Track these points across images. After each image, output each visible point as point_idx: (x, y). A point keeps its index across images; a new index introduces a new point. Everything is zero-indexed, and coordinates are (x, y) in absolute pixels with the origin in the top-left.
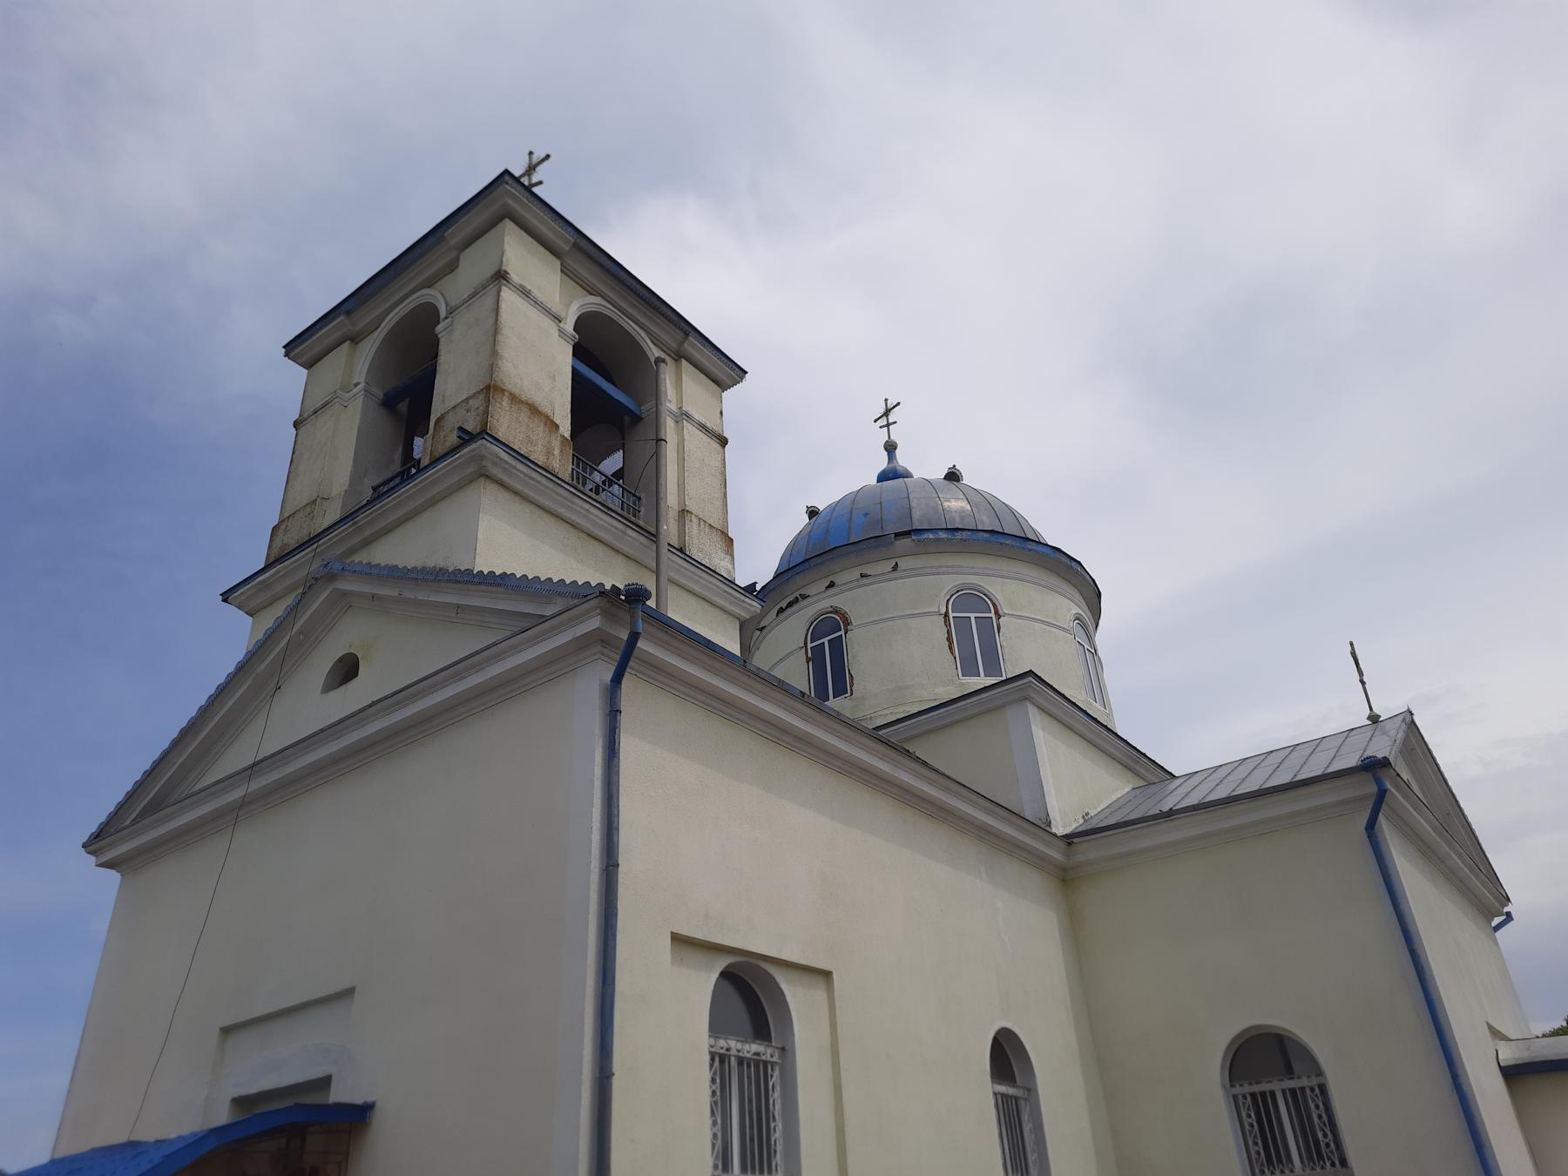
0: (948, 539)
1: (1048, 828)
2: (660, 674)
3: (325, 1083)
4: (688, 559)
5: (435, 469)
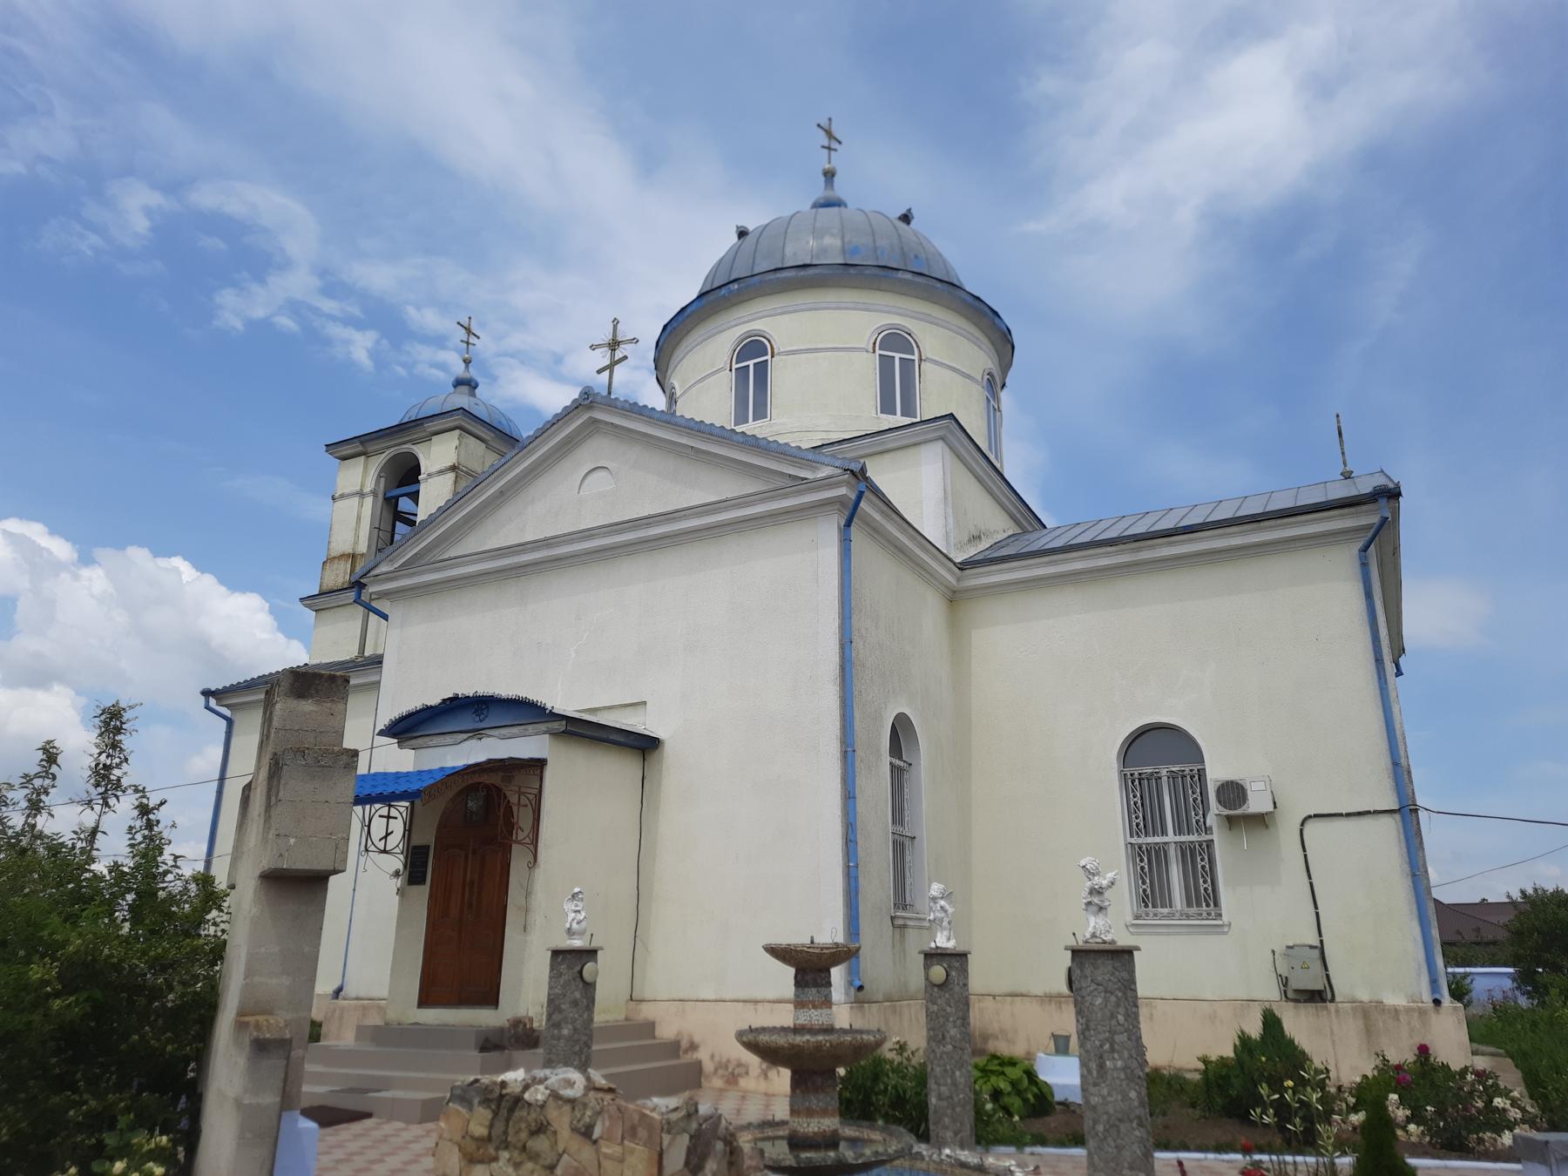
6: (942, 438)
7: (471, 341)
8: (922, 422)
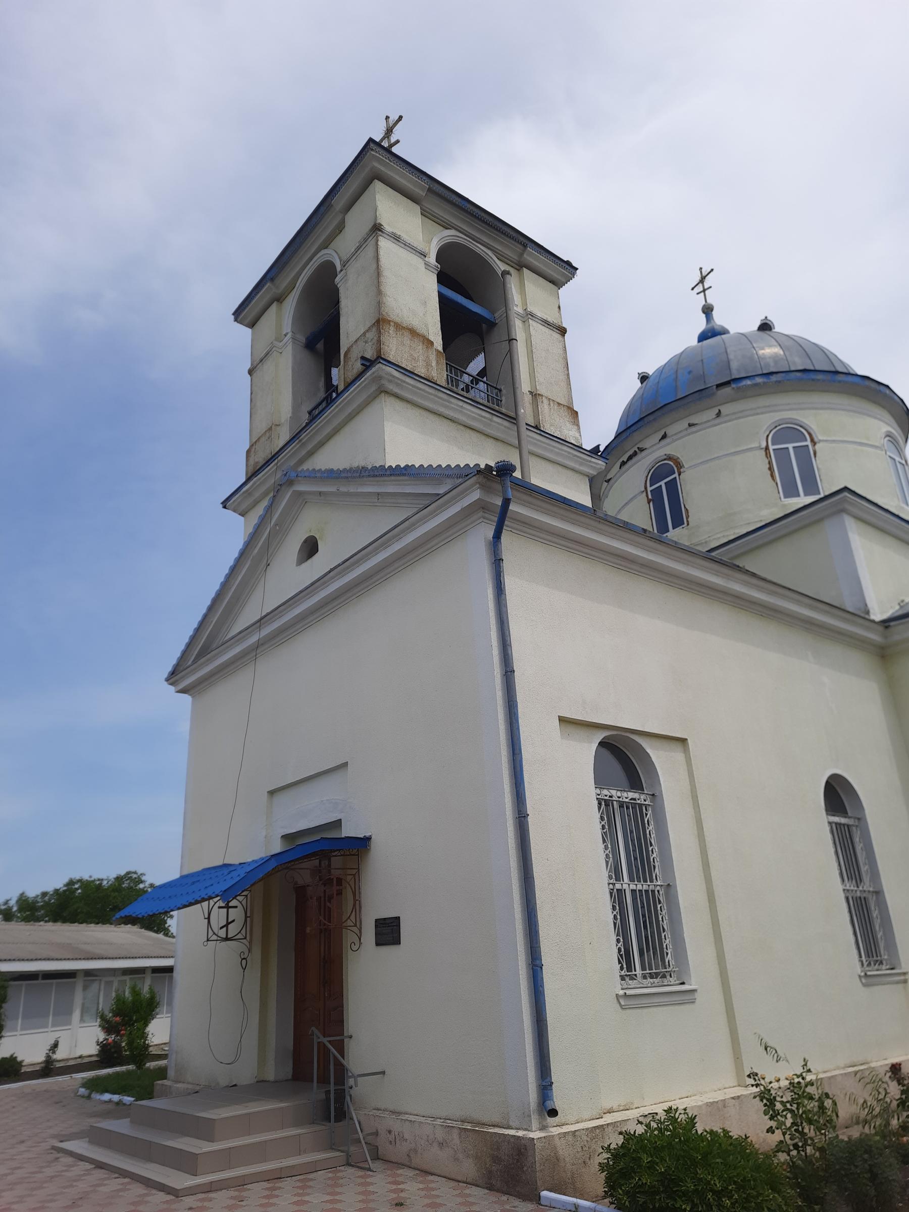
0: (764, 383)
1: (867, 616)
2: (530, 528)
3: (337, 824)
4: (543, 434)
5: (349, 392)
8: (826, 497)
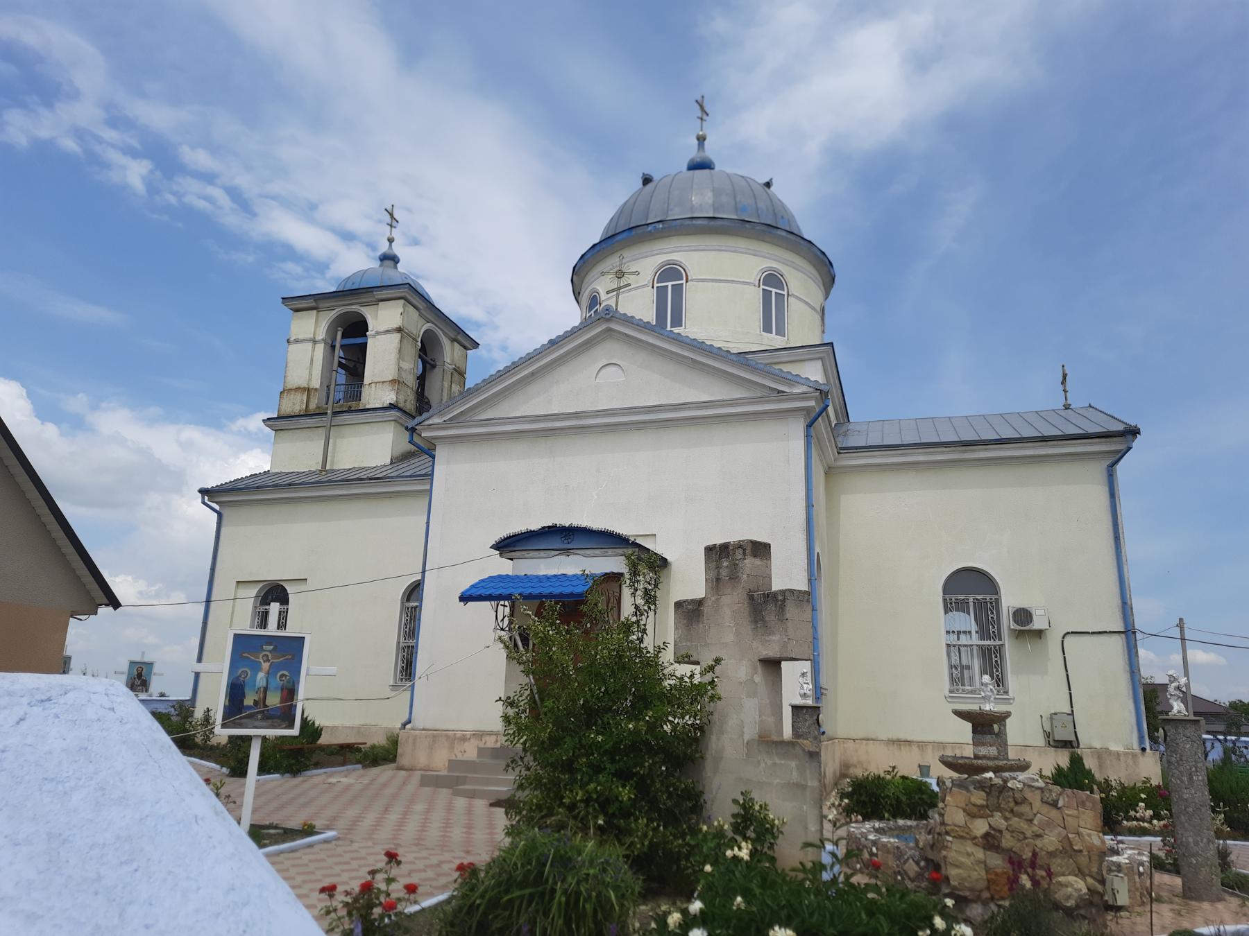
6: (820, 358)
7: (393, 224)
